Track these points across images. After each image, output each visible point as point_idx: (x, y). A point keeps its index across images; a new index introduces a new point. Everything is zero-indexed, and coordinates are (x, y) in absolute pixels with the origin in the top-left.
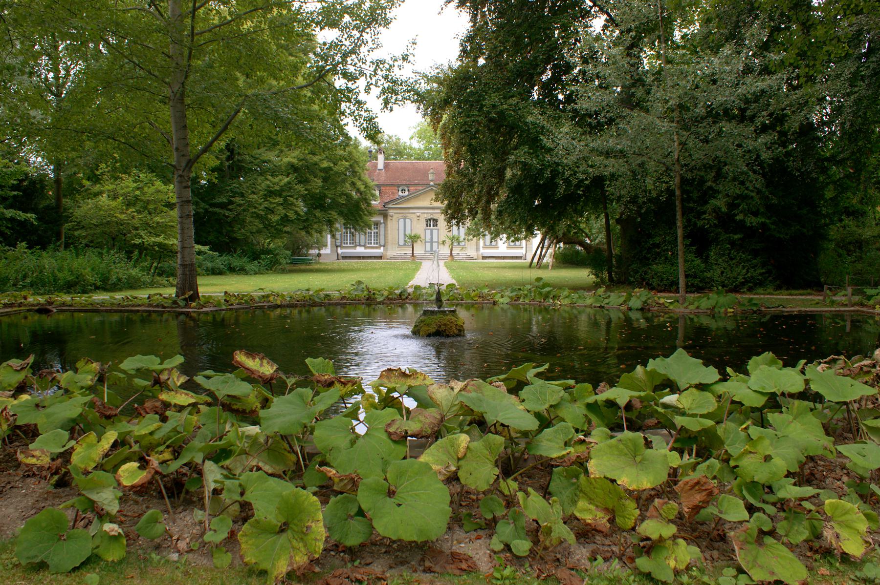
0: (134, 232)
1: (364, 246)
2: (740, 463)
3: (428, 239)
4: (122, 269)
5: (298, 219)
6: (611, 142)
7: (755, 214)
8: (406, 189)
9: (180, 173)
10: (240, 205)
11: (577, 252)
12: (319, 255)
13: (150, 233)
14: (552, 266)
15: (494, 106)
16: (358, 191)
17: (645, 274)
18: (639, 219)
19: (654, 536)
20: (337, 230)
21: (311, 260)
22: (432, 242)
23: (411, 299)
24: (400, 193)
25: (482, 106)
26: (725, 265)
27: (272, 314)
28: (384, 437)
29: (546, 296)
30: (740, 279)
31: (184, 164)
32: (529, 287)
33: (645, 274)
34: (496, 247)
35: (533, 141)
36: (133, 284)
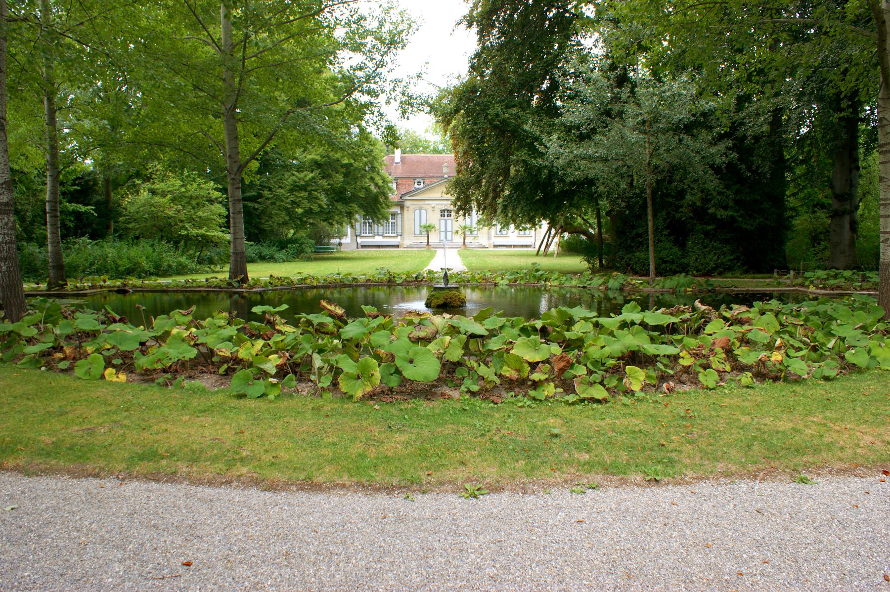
0: (180, 224)
1: (382, 235)
2: (588, 350)
3: (443, 229)
4: (171, 258)
5: (321, 211)
6: (590, 152)
7: (725, 208)
8: (422, 182)
9: (233, 176)
10: (268, 199)
11: (581, 241)
12: (340, 244)
13: (194, 225)
14: (557, 254)
15: (497, 115)
16: (376, 185)
17: (630, 260)
18: (628, 212)
19: (537, 379)
20: (356, 220)
21: (333, 249)
22: (446, 231)
23: (426, 281)
24: (416, 186)
25: (487, 114)
26: (699, 252)
27: (309, 294)
28: (407, 340)
29: (539, 279)
30: (712, 265)
31: (235, 169)
32: (525, 271)
33: (630, 260)
34: (507, 236)
35: (531, 144)
36: (181, 270)
